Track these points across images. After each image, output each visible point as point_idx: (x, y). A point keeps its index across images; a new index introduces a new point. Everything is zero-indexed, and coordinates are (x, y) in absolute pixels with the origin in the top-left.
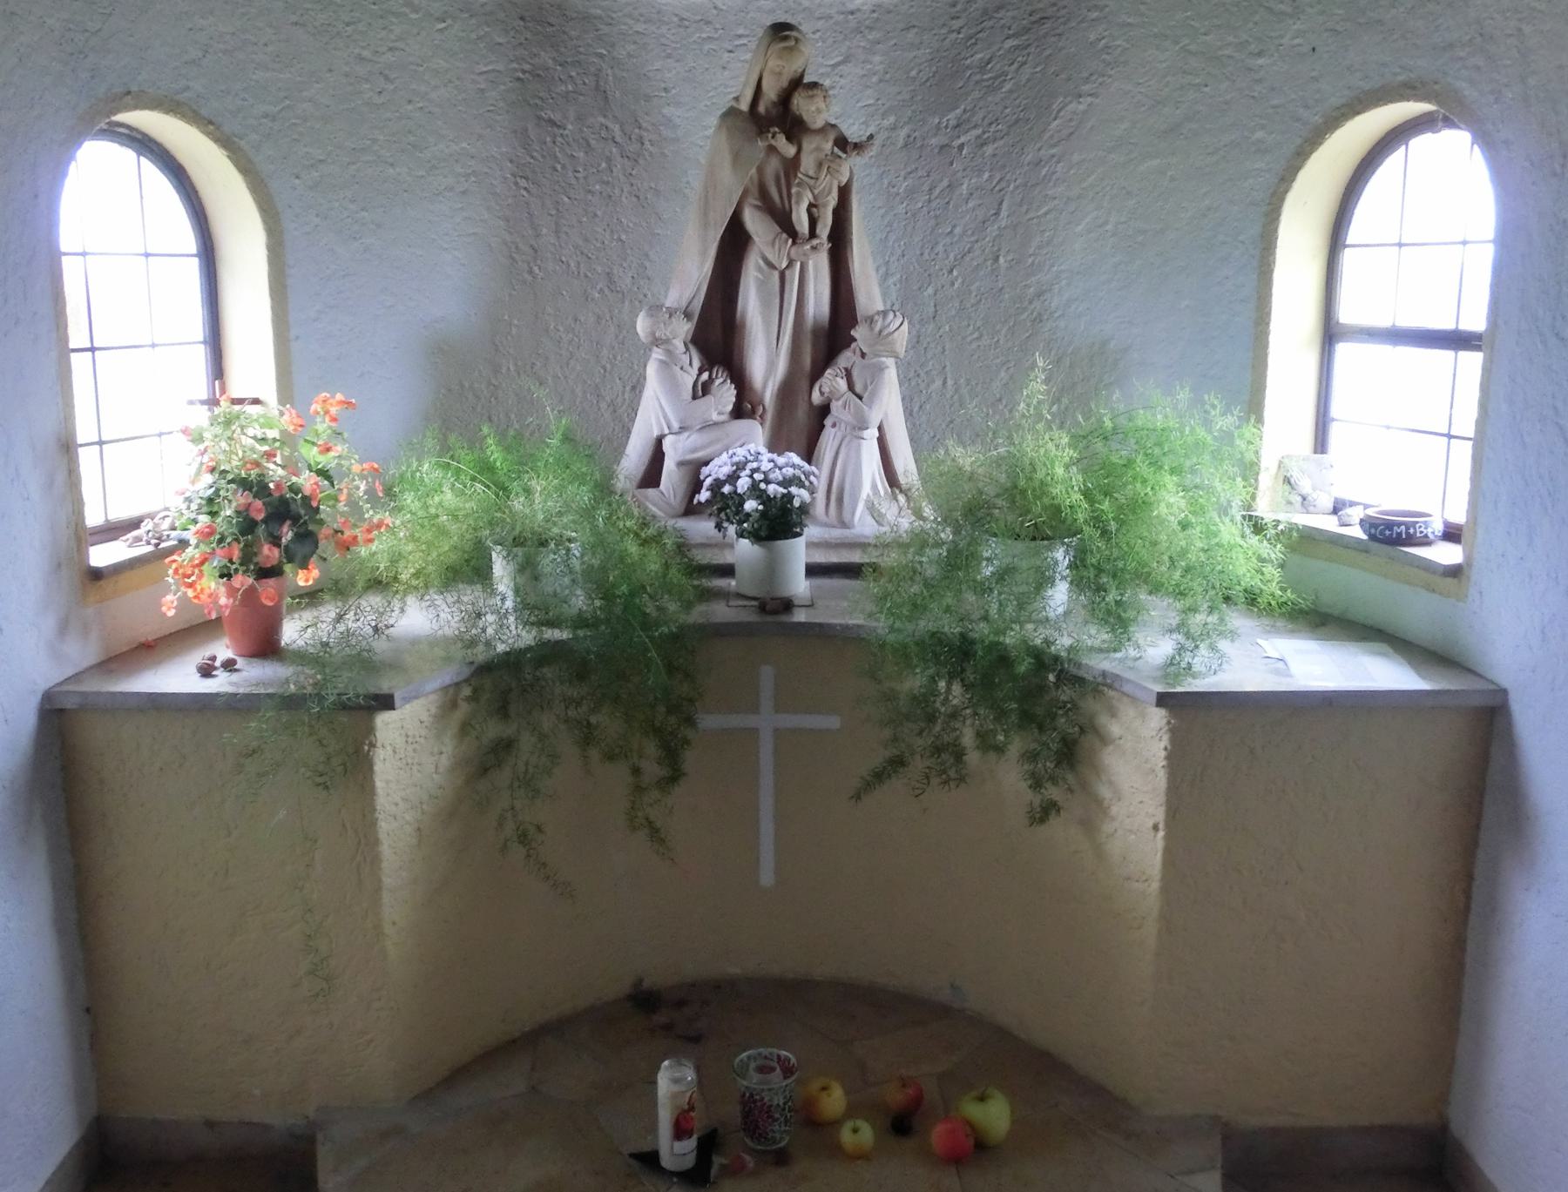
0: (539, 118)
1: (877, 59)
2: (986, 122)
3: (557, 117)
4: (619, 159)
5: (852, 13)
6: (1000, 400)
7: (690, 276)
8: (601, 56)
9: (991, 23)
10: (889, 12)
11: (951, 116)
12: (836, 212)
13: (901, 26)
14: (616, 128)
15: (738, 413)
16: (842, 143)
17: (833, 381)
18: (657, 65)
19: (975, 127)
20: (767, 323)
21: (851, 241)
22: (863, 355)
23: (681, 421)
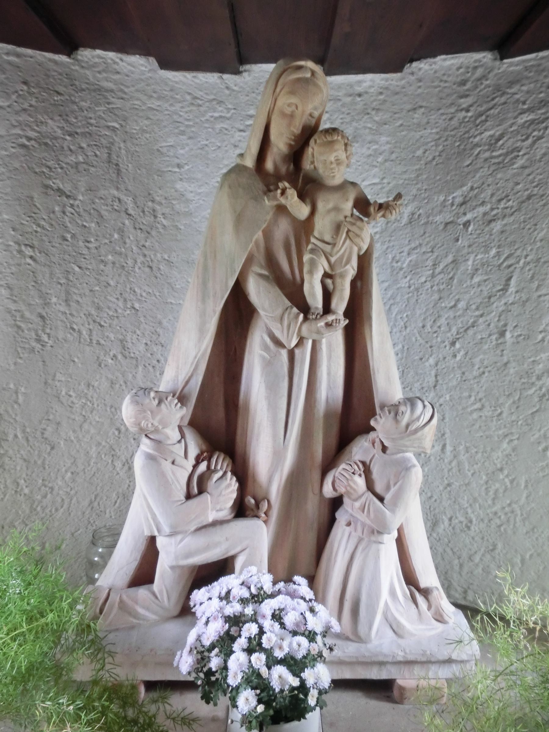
0: (47, 187)
1: (384, 139)
2: (494, 199)
3: (67, 188)
4: (132, 230)
5: (360, 95)
6: (501, 470)
7: (186, 351)
8: (114, 129)
9: (503, 99)
10: (397, 93)
11: (458, 193)
12: (353, 283)
13: (409, 107)
14: (129, 201)
15: (241, 510)
16: (363, 205)
17: (346, 478)
18: (171, 141)
19: (483, 203)
20: (272, 407)
21: (370, 318)
22: (384, 449)
23: (172, 527)
